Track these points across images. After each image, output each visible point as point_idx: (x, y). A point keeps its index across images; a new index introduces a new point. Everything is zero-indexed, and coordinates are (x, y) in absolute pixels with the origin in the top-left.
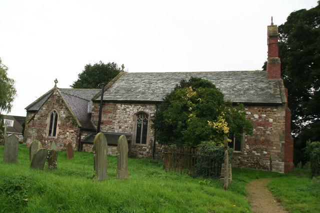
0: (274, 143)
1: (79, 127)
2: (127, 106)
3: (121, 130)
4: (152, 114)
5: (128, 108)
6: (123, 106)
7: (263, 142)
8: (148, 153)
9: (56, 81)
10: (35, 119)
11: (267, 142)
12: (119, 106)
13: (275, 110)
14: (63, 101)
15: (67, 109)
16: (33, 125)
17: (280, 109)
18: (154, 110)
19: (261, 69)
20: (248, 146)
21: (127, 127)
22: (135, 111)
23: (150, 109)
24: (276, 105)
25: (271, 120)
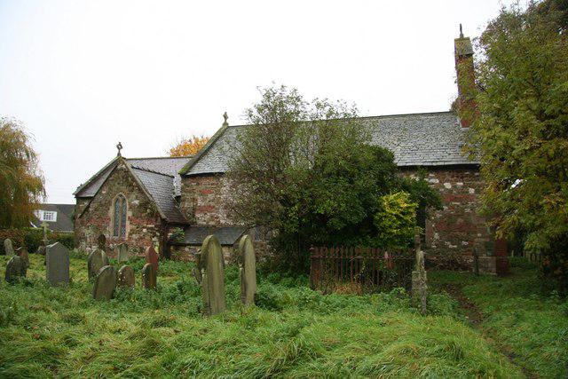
7: (460, 228)
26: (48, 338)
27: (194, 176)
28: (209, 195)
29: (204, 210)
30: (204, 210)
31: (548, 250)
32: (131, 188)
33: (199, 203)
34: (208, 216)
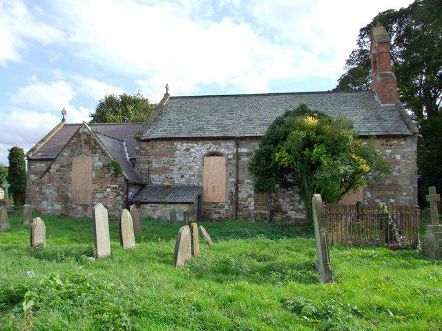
0: (403, 187)
1: (126, 180)
2: (190, 145)
3: (183, 180)
4: (230, 154)
5: (192, 147)
6: (185, 144)
7: (389, 187)
8: (227, 210)
9: (64, 113)
10: (51, 170)
11: (395, 186)
12: (178, 145)
13: (403, 143)
14: (95, 142)
15: (103, 153)
16: (50, 181)
17: (409, 140)
18: (233, 150)
19: (150, 103)
20: (368, 193)
21: (193, 176)
22: (204, 151)
23: (227, 147)
24: (405, 137)
25: (398, 157)
26: (270, 259)
27: (148, 141)
28: (164, 158)
29: (158, 171)
30: (158, 171)
31: (43, 248)
32: (94, 150)
33: (155, 165)
34: (163, 177)
